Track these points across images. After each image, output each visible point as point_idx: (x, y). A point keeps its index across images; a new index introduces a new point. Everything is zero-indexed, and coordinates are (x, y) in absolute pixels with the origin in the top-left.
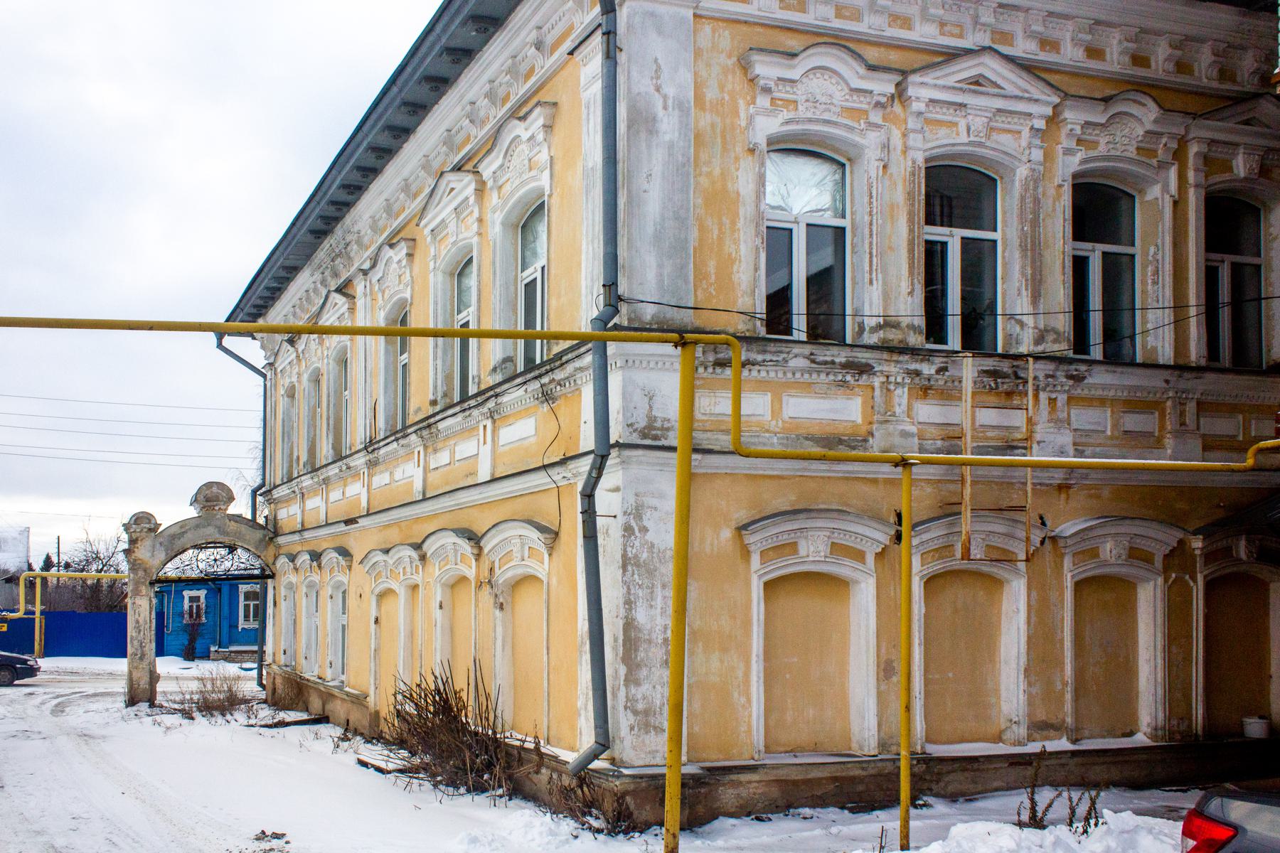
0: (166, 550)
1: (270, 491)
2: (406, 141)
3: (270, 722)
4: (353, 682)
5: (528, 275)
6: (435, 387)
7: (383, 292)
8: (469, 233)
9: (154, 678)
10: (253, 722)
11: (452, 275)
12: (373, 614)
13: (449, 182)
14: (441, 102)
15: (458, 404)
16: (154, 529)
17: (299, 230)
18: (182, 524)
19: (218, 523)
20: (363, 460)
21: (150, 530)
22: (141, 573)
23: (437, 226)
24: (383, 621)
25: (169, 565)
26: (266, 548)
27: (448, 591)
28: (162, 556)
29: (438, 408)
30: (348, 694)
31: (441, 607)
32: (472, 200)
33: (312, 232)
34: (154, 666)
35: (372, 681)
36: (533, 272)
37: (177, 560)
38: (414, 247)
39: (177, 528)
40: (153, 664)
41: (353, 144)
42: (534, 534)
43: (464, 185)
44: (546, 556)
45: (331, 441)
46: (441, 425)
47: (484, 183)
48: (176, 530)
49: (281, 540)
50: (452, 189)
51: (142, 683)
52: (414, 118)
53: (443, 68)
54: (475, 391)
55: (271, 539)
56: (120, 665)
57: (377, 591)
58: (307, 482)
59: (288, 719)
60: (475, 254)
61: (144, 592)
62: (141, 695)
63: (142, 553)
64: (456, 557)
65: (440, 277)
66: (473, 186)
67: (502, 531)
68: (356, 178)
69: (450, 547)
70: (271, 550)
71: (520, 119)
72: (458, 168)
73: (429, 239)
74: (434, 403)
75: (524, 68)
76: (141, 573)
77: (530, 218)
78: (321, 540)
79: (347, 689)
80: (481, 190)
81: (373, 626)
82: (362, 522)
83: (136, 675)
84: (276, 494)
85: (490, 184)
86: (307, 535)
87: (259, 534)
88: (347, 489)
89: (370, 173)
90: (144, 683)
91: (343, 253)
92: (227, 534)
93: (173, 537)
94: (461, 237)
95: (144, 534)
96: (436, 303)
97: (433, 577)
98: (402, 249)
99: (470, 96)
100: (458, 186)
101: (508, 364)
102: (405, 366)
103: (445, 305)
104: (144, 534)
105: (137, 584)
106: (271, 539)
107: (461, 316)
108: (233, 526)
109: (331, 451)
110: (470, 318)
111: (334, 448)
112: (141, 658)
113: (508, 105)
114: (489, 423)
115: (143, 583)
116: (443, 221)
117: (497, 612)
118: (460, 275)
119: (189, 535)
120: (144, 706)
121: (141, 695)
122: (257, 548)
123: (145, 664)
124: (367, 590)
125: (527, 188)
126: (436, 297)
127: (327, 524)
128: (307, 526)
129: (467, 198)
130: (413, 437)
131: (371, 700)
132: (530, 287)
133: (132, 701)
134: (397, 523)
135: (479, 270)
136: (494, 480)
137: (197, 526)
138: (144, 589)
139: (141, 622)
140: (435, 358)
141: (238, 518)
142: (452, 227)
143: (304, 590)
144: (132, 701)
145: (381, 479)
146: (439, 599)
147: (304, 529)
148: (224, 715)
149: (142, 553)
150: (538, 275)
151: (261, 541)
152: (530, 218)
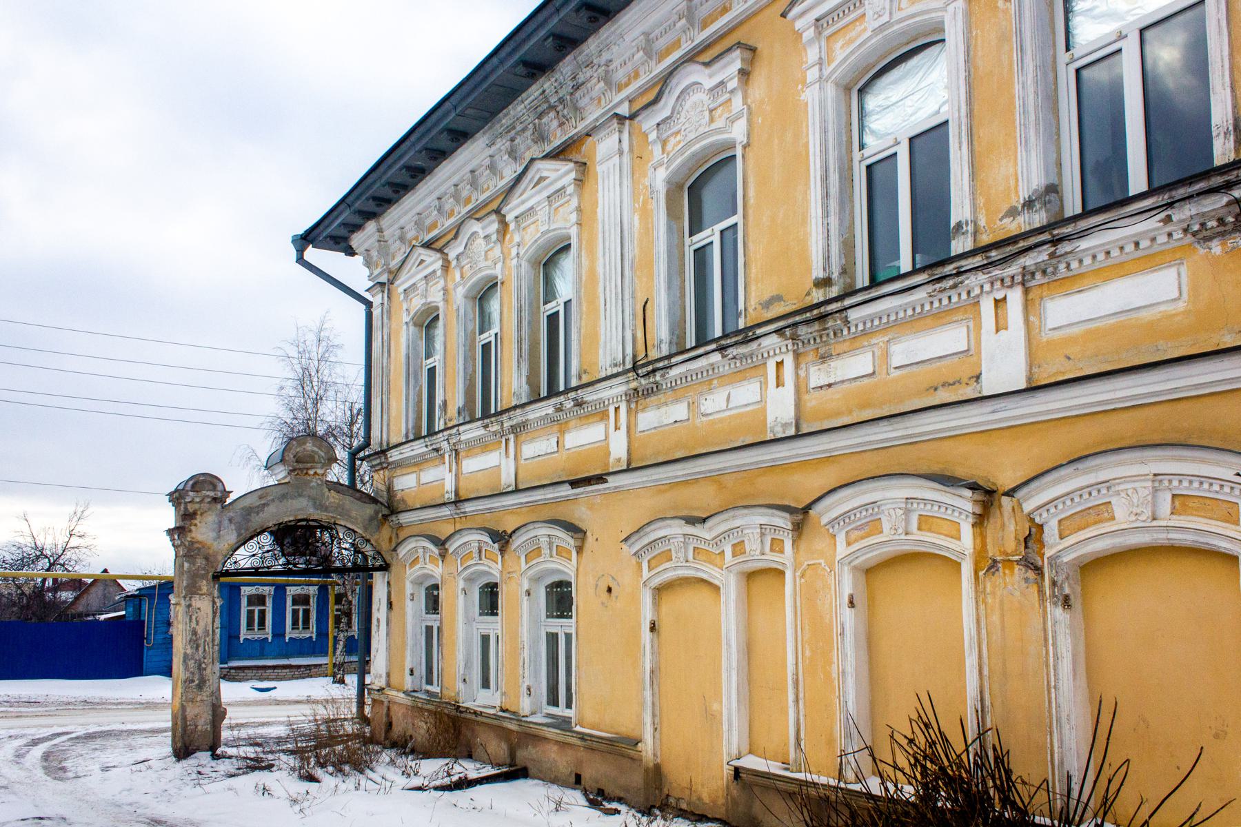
0: (238, 530)
1: (383, 452)
2: (421, 180)
3: (447, 781)
4: (590, 716)
5: (551, 308)
6: (827, 258)
7: (664, 144)
8: (436, 297)
9: (218, 713)
10: (417, 782)
11: (848, 89)
12: (647, 615)
13: (538, 170)
14: (602, 30)
15: (479, 419)
16: (220, 498)
17: (502, 62)
18: (263, 492)
19: (313, 493)
20: (622, 389)
21: (215, 500)
22: (200, 562)
23: (522, 214)
24: (664, 626)
25: (241, 551)
26: (379, 528)
27: (862, 578)
28: (231, 537)
29: (834, 291)
30: (583, 737)
31: (852, 604)
32: (439, 273)
33: (525, 63)
34: (219, 698)
35: (648, 719)
36: (557, 306)
37: (252, 543)
38: (583, 173)
39: (256, 495)
40: (216, 694)
41: (335, 213)
42: (559, 533)
43: (433, 261)
44: (574, 554)
45: (524, 372)
46: (853, 315)
47: (449, 262)
48: (253, 501)
49: (405, 518)
50: (422, 261)
51: (201, 722)
52: (454, 144)
53: (444, 142)
54: (442, 427)
55: (385, 517)
56: (156, 689)
57: (656, 582)
58: (473, 432)
59: (473, 775)
60: (441, 312)
61: (205, 589)
62: (195, 740)
63: (203, 531)
64: (550, 549)
65: (831, 91)
66: (440, 263)
67: (1097, 469)
68: (404, 177)
69: (544, 540)
70: (386, 532)
71: (478, 219)
72: (428, 245)
73: (402, 297)
74: (825, 282)
75: (428, 222)
76: (200, 562)
77: (484, 292)
78: (508, 512)
79: (578, 729)
80: (446, 267)
81: (646, 635)
82: (613, 482)
83: (191, 711)
84: (394, 455)
85: (454, 263)
86: (469, 507)
87: (369, 509)
88: (640, 416)
89: (401, 189)
90: (203, 724)
91: (567, 106)
92: (326, 509)
93: (249, 512)
94: (898, 16)
95: (205, 506)
96: (824, 131)
97: (837, 556)
98: (734, 62)
99: (402, 222)
100: (429, 260)
101: (1053, 197)
102: (486, 348)
103: (839, 134)
104: (205, 506)
105: (194, 577)
106: (385, 517)
107: (483, 337)
108: (333, 497)
109: (525, 387)
110: (436, 364)
111: (529, 382)
112: (200, 687)
113: (469, 207)
114: (512, 437)
115: (203, 577)
116: (532, 208)
117: (1059, 612)
118: (861, 91)
119: (271, 509)
120: (204, 757)
121: (195, 740)
122: (366, 529)
123: (204, 695)
124: (626, 580)
125: (479, 275)
126: (824, 121)
127: (517, 490)
128: (463, 495)
129: (434, 272)
130: (774, 340)
131: (647, 748)
132: (486, 348)
133: (182, 752)
134: (715, 478)
135: (445, 326)
136: (1033, 389)
137: (284, 497)
138: (204, 586)
139: (200, 631)
140: (826, 214)
141: (335, 487)
142: (542, 214)
143: (461, 584)
144: (182, 752)
145: (649, 419)
146: (847, 590)
147: (458, 501)
148: (362, 772)
149: (203, 531)
150: (493, 339)
151: (371, 519)
152: (484, 292)
